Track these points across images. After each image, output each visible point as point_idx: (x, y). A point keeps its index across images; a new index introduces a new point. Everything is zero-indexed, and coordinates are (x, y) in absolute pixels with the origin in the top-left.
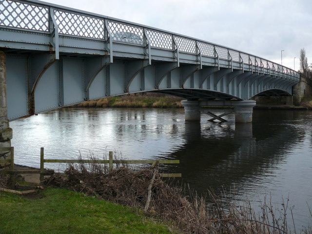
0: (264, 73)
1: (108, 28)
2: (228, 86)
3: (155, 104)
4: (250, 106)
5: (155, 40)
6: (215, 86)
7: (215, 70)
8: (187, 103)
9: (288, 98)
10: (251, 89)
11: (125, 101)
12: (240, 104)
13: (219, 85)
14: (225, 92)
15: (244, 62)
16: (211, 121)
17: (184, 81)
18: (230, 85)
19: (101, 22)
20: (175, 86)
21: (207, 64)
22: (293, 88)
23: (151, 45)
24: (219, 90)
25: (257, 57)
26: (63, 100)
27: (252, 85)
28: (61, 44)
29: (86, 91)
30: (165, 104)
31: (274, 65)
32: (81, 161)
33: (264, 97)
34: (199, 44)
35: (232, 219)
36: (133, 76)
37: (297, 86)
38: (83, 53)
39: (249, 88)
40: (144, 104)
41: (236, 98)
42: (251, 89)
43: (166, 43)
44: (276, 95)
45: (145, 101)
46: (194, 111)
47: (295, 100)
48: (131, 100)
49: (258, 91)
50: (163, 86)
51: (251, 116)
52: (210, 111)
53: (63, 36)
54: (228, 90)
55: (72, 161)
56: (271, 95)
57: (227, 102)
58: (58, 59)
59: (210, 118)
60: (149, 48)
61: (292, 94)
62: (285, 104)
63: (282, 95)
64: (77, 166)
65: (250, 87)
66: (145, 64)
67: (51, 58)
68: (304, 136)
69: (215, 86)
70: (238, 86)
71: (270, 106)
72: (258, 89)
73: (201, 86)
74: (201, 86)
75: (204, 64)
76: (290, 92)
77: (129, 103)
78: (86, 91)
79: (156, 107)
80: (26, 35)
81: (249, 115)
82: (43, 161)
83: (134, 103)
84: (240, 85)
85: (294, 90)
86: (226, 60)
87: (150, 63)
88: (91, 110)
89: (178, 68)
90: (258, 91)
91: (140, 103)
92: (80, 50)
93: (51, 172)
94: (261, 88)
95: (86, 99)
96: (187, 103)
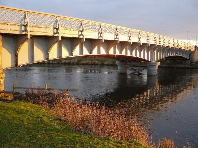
0: (175, 47)
3: (105, 63)
8: (119, 63)
9: (187, 61)
11: (87, 61)
12: (149, 64)
13: (134, 52)
14: (138, 56)
16: (133, 74)
18: (142, 52)
22: (190, 55)
24: (134, 55)
27: (159, 53)
30: (111, 63)
32: (32, 89)
33: (172, 60)
36: (95, 47)
37: (193, 54)
40: (99, 63)
41: (146, 60)
44: (179, 59)
45: (99, 61)
46: (123, 67)
47: (191, 63)
48: (91, 60)
51: (156, 71)
52: (133, 68)
55: (28, 89)
56: (177, 59)
59: (133, 72)
61: (190, 58)
62: (185, 65)
63: (183, 59)
64: (30, 91)
67: (26, 38)
68: (31, 70)
71: (175, 66)
72: (163, 54)
73: (121, 53)
76: (188, 57)
77: (90, 62)
79: (106, 65)
82: (14, 88)
83: (93, 62)
84: (149, 53)
85: (191, 56)
88: (67, 66)
91: (96, 62)
93: (18, 93)
94: (165, 55)
96: (119, 63)
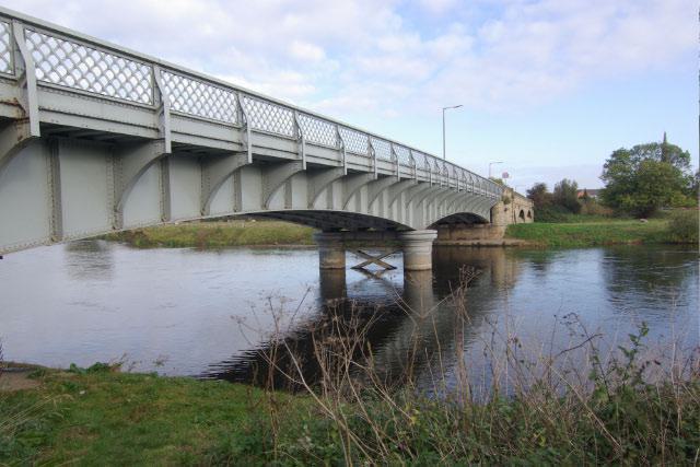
1: (243, 106)
2: (390, 206)
4: (426, 240)
5: (312, 131)
6: (370, 206)
7: (371, 177)
10: (428, 211)
13: (375, 205)
14: (386, 216)
15: (252, 125)
17: (315, 197)
19: (232, 96)
20: (299, 203)
21: (355, 168)
23: (253, 124)
25: (302, 112)
26: (60, 225)
28: (255, 143)
29: (117, 210)
31: (375, 143)
34: (343, 132)
35: (527, 257)
38: (116, 131)
39: (425, 210)
42: (428, 211)
43: (283, 123)
49: (439, 214)
50: (277, 204)
53: (42, 86)
54: (407, 218)
57: (393, 236)
58: (38, 134)
59: (360, 262)
60: (249, 130)
65: (428, 206)
66: (20, 132)
69: (370, 206)
70: (407, 205)
73: (345, 205)
74: (345, 205)
75: (351, 167)
76: (487, 217)
78: (117, 210)
80: (81, 100)
81: (423, 256)
84: (411, 205)
86: (230, 127)
87: (250, 161)
89: (33, 139)
90: (439, 214)
92: (61, 116)
95: (118, 222)
